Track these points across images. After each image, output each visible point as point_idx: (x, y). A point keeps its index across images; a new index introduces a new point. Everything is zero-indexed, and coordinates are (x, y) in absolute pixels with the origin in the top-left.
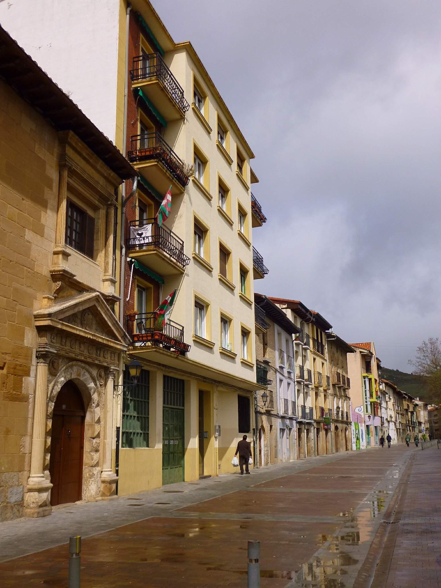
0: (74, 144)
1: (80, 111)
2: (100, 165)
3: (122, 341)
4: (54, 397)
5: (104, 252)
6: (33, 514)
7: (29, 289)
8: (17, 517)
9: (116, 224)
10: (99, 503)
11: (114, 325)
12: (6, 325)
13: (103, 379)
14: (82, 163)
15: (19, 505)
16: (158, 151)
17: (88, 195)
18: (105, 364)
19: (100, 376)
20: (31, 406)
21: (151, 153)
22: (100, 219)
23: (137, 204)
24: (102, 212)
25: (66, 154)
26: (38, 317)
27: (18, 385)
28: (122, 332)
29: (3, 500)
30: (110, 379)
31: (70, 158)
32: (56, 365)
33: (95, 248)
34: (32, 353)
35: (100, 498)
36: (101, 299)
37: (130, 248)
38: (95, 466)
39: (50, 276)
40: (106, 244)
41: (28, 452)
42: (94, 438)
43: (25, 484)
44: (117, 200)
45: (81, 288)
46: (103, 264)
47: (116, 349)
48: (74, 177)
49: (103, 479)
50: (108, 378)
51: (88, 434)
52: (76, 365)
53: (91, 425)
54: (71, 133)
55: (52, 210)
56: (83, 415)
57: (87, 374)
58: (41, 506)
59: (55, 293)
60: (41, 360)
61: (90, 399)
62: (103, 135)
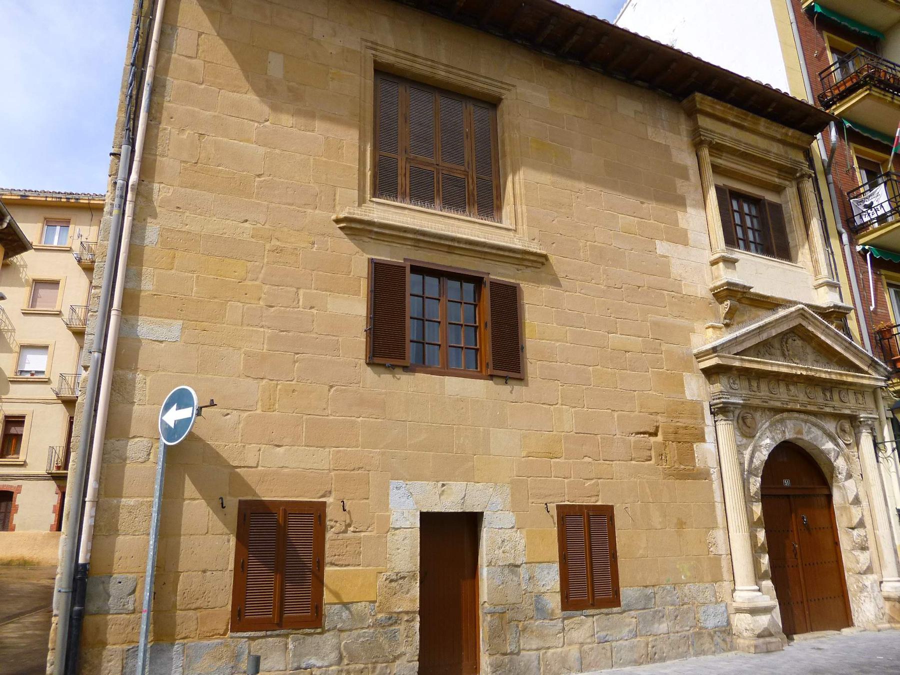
0: (709, 110)
1: (698, 60)
2: (763, 125)
3: (870, 371)
4: (757, 469)
5: (807, 246)
6: (748, 647)
7: (678, 319)
8: (724, 651)
9: (820, 202)
10: (882, 635)
11: (846, 349)
12: (649, 374)
13: (850, 434)
14: (733, 132)
15: (724, 631)
16: (865, 73)
17: (758, 174)
18: (847, 412)
19: (843, 431)
20: (716, 485)
21: (855, 81)
22: (789, 201)
23: (856, 165)
24: (791, 192)
25: (699, 127)
26: (699, 356)
27: (688, 456)
28: (867, 359)
29: (694, 624)
30: (864, 434)
31: (707, 130)
32: (748, 421)
33: (791, 244)
34: (703, 409)
35: (887, 625)
36: (810, 314)
37: (855, 230)
38: (865, 573)
39: (711, 296)
40: (808, 235)
41: (724, 553)
42: (853, 529)
43: (728, 600)
44: (812, 166)
45: (768, 304)
46: (810, 264)
47: (862, 385)
48: (724, 154)
49: (886, 594)
50: (860, 432)
51: (841, 522)
52: (790, 419)
53: (844, 508)
54: (698, 96)
55: (694, 206)
56: (827, 492)
57: (814, 429)
58: (759, 636)
59: (725, 318)
60: (720, 417)
61: (832, 468)
62: (771, 89)
